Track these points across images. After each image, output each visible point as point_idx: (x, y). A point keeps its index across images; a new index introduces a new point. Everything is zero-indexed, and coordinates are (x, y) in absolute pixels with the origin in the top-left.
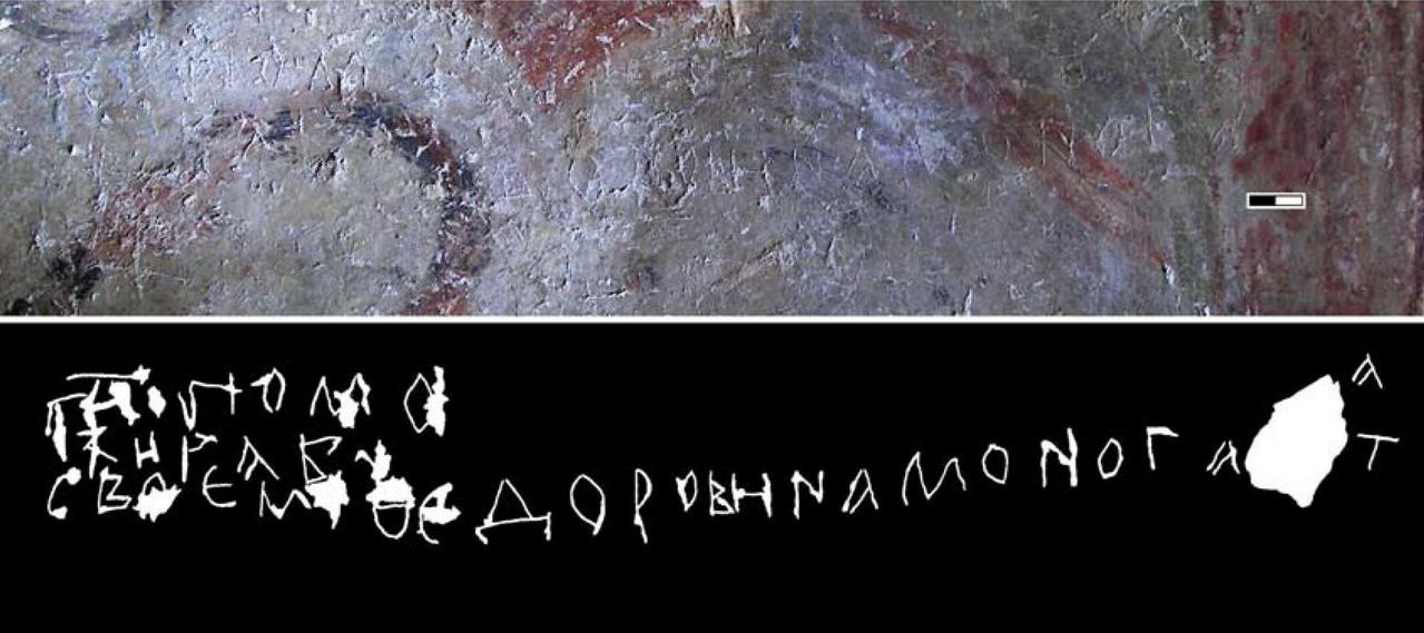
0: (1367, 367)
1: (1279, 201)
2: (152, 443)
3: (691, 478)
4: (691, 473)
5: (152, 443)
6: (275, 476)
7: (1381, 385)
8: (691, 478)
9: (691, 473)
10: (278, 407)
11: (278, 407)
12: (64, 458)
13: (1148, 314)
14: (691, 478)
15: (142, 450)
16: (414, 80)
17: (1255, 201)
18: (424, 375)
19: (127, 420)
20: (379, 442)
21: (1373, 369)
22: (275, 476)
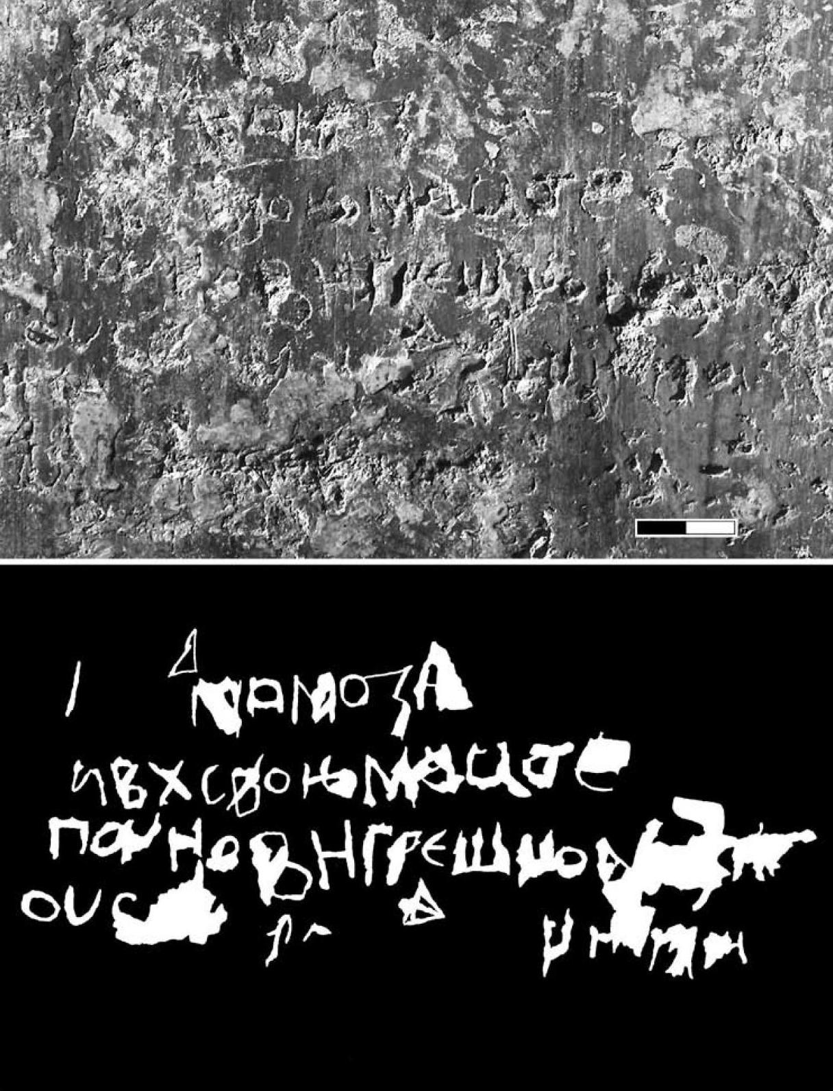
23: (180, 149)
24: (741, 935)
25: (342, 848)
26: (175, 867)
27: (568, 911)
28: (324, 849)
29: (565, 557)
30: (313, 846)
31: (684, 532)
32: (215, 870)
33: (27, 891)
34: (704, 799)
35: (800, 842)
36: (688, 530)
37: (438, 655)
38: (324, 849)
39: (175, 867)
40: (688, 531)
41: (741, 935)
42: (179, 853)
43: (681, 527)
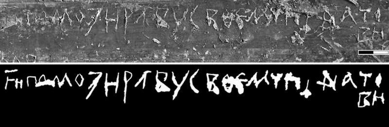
0: (348, 78)
1: (374, 52)
2: (107, 90)
3: (56, 79)
4: (56, 77)
5: (107, 90)
6: (28, 84)
7: (308, 81)
8: (56, 79)
9: (56, 77)
10: (78, 75)
11: (78, 75)
12: (165, 80)
13: (352, 62)
14: (56, 79)
15: (109, 81)
16: (269, 38)
17: (360, 52)
18: (58, 77)
19: (51, 86)
20: (334, 89)
21: (350, 79)
22: (28, 84)
30: (101, 78)
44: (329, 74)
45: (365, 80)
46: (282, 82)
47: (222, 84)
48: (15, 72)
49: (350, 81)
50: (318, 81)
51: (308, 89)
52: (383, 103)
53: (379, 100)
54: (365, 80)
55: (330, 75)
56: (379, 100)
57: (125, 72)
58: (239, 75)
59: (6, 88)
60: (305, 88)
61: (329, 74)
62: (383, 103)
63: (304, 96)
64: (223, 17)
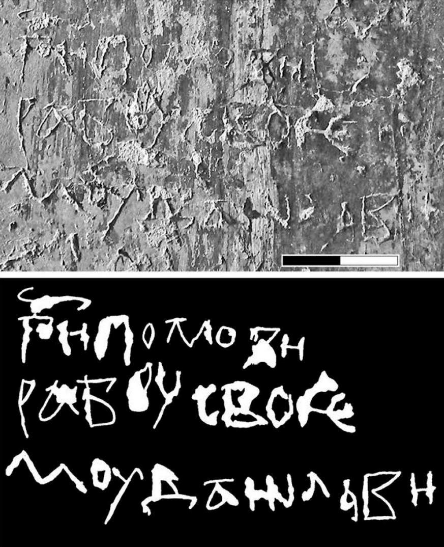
19: (211, 324)
23: (379, 188)
24: (415, 501)
25: (126, 479)
26: (77, 413)
27: (431, 502)
28: (124, 483)
29: (407, 270)
30: (197, 409)
31: (339, 263)
32: (108, 317)
33: (38, 419)
34: (198, 409)
35: (152, 502)
36: (342, 263)
37: (440, 275)
38: (124, 483)
39: (77, 413)
40: (341, 263)
41: (415, 501)
42: (216, 492)
43: (336, 261)
44: (82, 483)
45: (59, 408)
46: (302, 485)
47: (292, 416)
48: (25, 436)
49: (174, 493)
50: (250, 510)
51: (325, 409)
52: (245, 366)
53: (293, 353)
54: (59, 408)
55: (84, 484)
56: (293, 353)
57: (63, 466)
58: (23, 291)
59: (168, 340)
60: (325, 415)
61: (82, 483)
62: (245, 366)
63: (206, 386)
64: (399, 65)
